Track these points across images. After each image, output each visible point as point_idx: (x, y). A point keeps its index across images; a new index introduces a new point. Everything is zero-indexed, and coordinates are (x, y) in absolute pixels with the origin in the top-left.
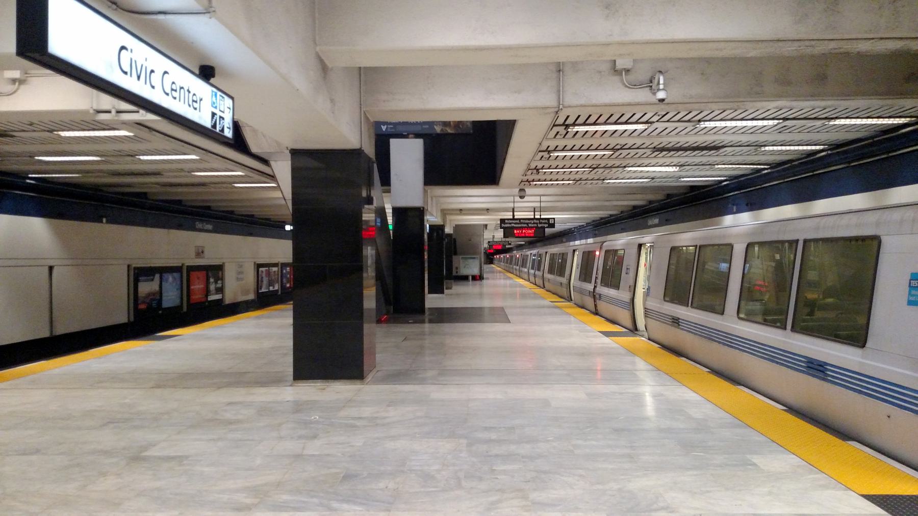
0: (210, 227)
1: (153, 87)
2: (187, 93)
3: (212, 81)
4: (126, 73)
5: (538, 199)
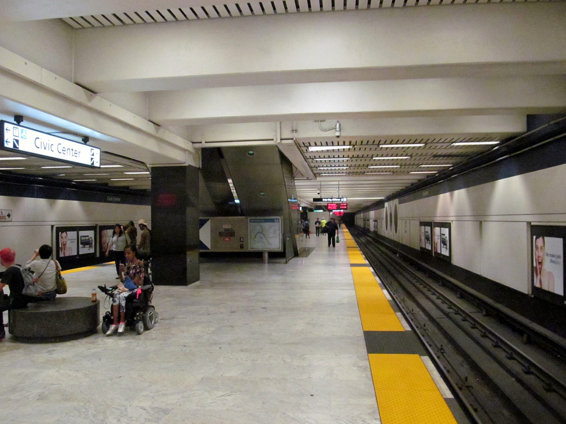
0: (118, 199)
1: (52, 151)
2: (71, 151)
3: (88, 143)
4: (38, 148)
5: (337, 183)
